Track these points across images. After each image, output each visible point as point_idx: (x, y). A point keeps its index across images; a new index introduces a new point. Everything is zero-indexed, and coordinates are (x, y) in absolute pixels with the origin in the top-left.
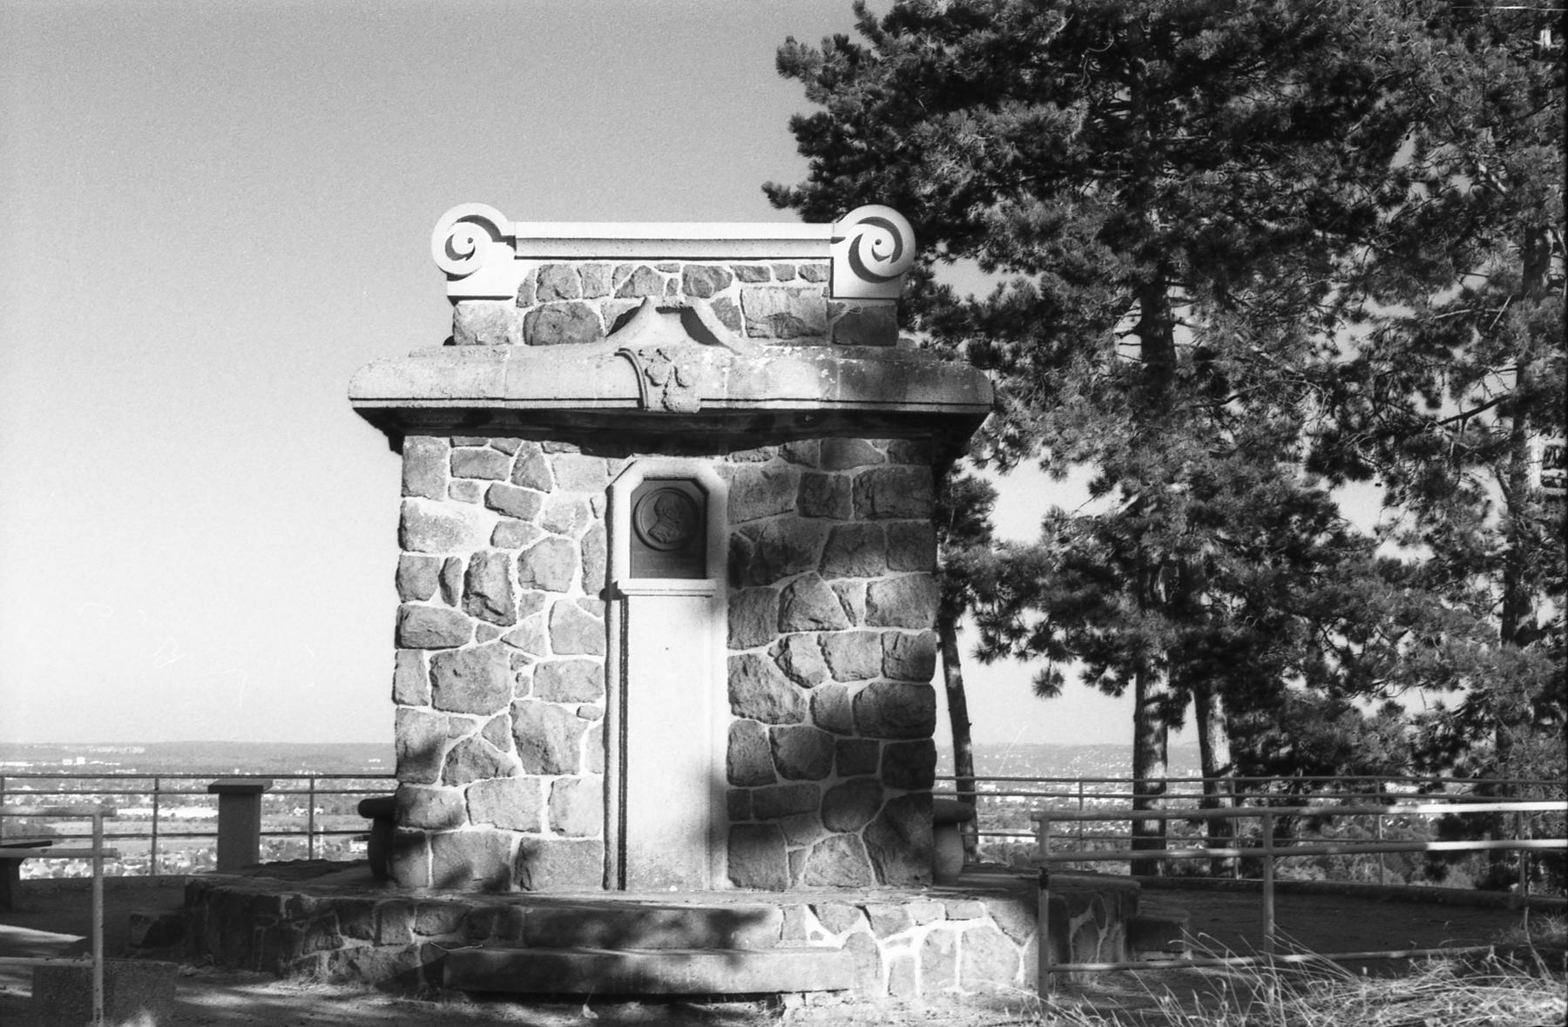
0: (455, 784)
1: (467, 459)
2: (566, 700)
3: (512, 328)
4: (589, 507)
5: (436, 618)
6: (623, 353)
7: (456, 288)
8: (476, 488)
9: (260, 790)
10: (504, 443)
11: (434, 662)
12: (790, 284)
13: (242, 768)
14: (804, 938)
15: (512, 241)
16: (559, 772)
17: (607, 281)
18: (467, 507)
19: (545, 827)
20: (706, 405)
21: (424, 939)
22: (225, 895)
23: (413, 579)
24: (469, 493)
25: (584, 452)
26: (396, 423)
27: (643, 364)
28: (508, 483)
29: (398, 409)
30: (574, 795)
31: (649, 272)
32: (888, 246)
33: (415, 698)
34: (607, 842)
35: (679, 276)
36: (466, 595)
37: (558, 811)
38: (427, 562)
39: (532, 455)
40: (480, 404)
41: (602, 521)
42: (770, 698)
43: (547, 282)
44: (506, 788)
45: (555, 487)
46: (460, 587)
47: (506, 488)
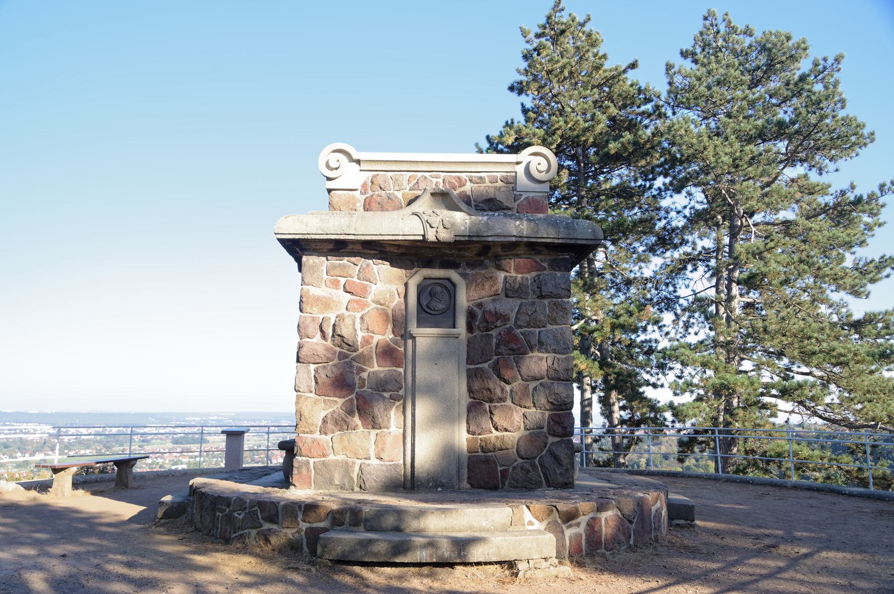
0: (326, 434)
1: (334, 267)
2: (384, 391)
3: (358, 205)
4: (396, 292)
5: (317, 347)
6: (414, 214)
7: (330, 185)
8: (339, 281)
9: (243, 432)
10: (353, 259)
11: (316, 371)
12: (496, 184)
13: (234, 425)
14: (524, 525)
15: (358, 162)
16: (380, 428)
17: (405, 182)
18: (334, 291)
19: (373, 457)
20: (458, 238)
21: (308, 525)
22: (203, 494)
23: (306, 328)
24: (336, 284)
25: (392, 265)
26: (297, 248)
27: (425, 218)
28: (355, 279)
29: (300, 239)
30: (389, 440)
31: (426, 178)
32: (544, 166)
33: (306, 389)
34: (405, 465)
35: (441, 180)
36: (333, 336)
37: (380, 449)
38: (313, 319)
39: (368, 265)
40: (342, 237)
41: (402, 300)
42: (490, 390)
43: (375, 182)
44: (352, 436)
45: (379, 283)
46: (330, 332)
47: (354, 282)
